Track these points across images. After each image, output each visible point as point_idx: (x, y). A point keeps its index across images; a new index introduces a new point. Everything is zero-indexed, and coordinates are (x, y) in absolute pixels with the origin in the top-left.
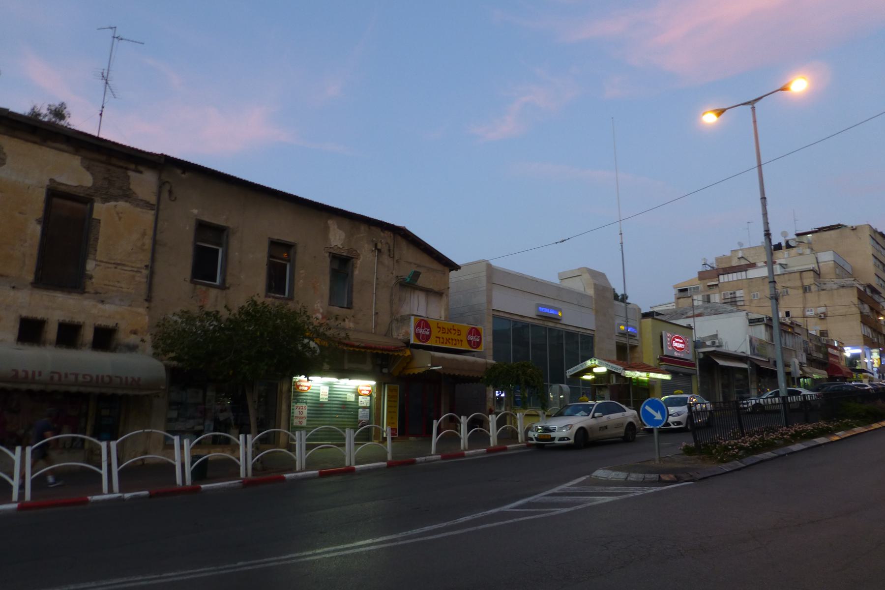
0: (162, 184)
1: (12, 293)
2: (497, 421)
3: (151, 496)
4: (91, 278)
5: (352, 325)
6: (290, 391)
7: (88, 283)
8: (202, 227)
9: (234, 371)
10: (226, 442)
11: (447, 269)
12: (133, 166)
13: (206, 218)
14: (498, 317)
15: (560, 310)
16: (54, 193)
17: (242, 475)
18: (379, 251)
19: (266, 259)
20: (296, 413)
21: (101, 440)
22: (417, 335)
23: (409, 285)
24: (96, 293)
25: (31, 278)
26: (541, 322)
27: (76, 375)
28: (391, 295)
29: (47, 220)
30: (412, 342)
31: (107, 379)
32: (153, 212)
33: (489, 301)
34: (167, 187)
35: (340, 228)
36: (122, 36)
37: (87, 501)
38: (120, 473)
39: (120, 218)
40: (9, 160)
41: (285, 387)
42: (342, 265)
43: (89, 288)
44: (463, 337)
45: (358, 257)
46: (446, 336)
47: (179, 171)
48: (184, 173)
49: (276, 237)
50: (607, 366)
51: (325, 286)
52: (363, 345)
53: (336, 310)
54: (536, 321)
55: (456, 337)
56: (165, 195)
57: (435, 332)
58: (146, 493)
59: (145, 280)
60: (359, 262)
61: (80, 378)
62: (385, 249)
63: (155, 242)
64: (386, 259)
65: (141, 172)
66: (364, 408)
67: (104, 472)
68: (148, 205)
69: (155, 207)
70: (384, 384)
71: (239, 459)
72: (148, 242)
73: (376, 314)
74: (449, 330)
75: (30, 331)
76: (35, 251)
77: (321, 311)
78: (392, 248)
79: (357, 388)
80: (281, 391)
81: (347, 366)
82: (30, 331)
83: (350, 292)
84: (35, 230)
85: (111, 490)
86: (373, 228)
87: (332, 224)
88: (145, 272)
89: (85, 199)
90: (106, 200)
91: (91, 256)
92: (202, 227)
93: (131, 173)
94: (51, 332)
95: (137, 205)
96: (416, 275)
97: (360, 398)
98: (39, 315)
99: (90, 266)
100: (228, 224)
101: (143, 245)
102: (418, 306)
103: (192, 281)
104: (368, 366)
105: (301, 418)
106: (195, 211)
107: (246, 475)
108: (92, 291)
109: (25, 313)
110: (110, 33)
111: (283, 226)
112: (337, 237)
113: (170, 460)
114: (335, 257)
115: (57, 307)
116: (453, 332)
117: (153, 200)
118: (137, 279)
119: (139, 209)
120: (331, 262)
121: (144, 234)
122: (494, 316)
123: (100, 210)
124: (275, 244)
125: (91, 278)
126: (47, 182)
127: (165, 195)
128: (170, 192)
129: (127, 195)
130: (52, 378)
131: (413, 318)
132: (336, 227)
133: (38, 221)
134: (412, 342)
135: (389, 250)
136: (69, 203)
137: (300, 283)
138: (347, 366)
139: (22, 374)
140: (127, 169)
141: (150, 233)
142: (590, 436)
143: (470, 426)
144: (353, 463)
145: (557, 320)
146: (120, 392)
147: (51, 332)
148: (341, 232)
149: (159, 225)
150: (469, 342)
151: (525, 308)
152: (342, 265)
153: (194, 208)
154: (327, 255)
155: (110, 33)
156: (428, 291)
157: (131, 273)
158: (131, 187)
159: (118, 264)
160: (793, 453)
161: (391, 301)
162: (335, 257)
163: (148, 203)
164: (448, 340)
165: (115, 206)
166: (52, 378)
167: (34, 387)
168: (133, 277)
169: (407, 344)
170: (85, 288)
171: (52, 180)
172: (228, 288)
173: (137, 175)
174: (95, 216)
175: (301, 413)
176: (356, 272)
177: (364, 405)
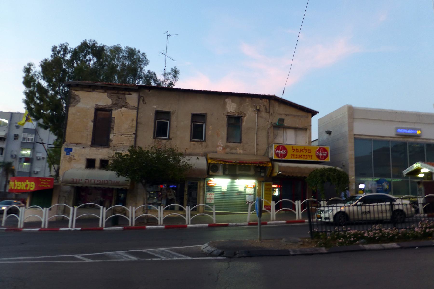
0: (139, 98)
1: (84, 150)
2: (302, 205)
3: (81, 230)
4: (112, 141)
5: (241, 151)
6: (204, 186)
7: (111, 143)
8: (158, 113)
9: (166, 178)
10: (181, 209)
11: (310, 115)
12: (128, 93)
13: (160, 109)
14: (359, 140)
15: (417, 129)
16: (98, 110)
17: (43, 226)
18: (259, 110)
19: (190, 123)
20: (208, 196)
21: (101, 205)
22: (277, 155)
23: (280, 126)
24: (114, 147)
25: (90, 143)
26: (401, 139)
27: (95, 180)
28: (268, 133)
29: (95, 121)
30: (274, 159)
31: (106, 182)
32: (136, 110)
33: (351, 129)
34: (142, 98)
35: (233, 102)
36: (171, 34)
37: (58, 230)
38: (77, 220)
39: (123, 115)
40: (81, 100)
41: (202, 184)
42: (234, 122)
43: (112, 144)
44: (313, 153)
45: (245, 115)
46: (298, 154)
47: (147, 91)
48: (149, 91)
49: (195, 112)
50: (429, 169)
51: (224, 133)
52: (238, 162)
53: (231, 144)
54: (396, 139)
55: (307, 154)
56: (141, 102)
57: (290, 152)
58: (80, 229)
59: (133, 139)
60: (245, 118)
61: (96, 182)
62: (263, 109)
63: (137, 123)
64: (264, 114)
65: (131, 94)
66: (250, 194)
67: (70, 219)
68: (134, 107)
69: (137, 108)
70: (263, 182)
71: (129, 218)
72: (134, 123)
73: (257, 144)
74: (302, 150)
75: (90, 164)
76: (91, 133)
77: (222, 145)
78: (268, 108)
79: (246, 185)
80: (200, 186)
81: (238, 173)
82: (90, 164)
83: (241, 134)
84: (91, 125)
85: (72, 227)
86: (254, 99)
87: (228, 101)
88: (134, 136)
89: (109, 110)
90: (117, 109)
91: (112, 132)
92: (158, 113)
93: (127, 96)
94: (97, 164)
95: (130, 109)
96: (281, 120)
97: (247, 189)
98: (93, 157)
99: (111, 136)
100: (171, 110)
101: (132, 125)
102: (289, 139)
103: (154, 137)
104: (252, 172)
105: (210, 199)
106: (155, 107)
107: (132, 225)
108: (112, 146)
109: (88, 157)
110: (166, 34)
111: (199, 107)
112: (231, 107)
113: (98, 216)
114: (230, 118)
115: (100, 153)
116: (305, 151)
117: (136, 105)
118: (130, 139)
119: (130, 110)
120: (228, 120)
121: (133, 120)
122: (355, 139)
123: (115, 113)
124: (194, 116)
125: (112, 141)
126: (95, 106)
127: (141, 102)
128: (143, 100)
129: (125, 105)
130: (86, 181)
131: (274, 145)
132: (231, 102)
133: (92, 121)
134: (274, 159)
135: (266, 109)
136: (104, 112)
137: (209, 133)
138: (238, 173)
139: (75, 180)
140: (125, 94)
141: (135, 119)
142: (352, 217)
143: (303, 207)
144: (104, 226)
145: (418, 136)
146: (111, 187)
147: (97, 164)
148: (233, 104)
149: (139, 116)
150: (318, 157)
151: (387, 131)
152: (234, 122)
153: (155, 104)
154: (226, 117)
155: (169, 33)
156: (296, 129)
157: (128, 137)
158: (127, 101)
159: (122, 134)
160: (364, 250)
161: (268, 137)
162: (230, 118)
163: (134, 107)
164: (300, 156)
165: (121, 111)
166: (86, 181)
167: (79, 185)
168: (128, 139)
169: (272, 160)
170: (109, 145)
171: (96, 105)
172: (171, 139)
173: (130, 96)
174: (113, 116)
175: (211, 197)
176: (244, 124)
177: (250, 193)
